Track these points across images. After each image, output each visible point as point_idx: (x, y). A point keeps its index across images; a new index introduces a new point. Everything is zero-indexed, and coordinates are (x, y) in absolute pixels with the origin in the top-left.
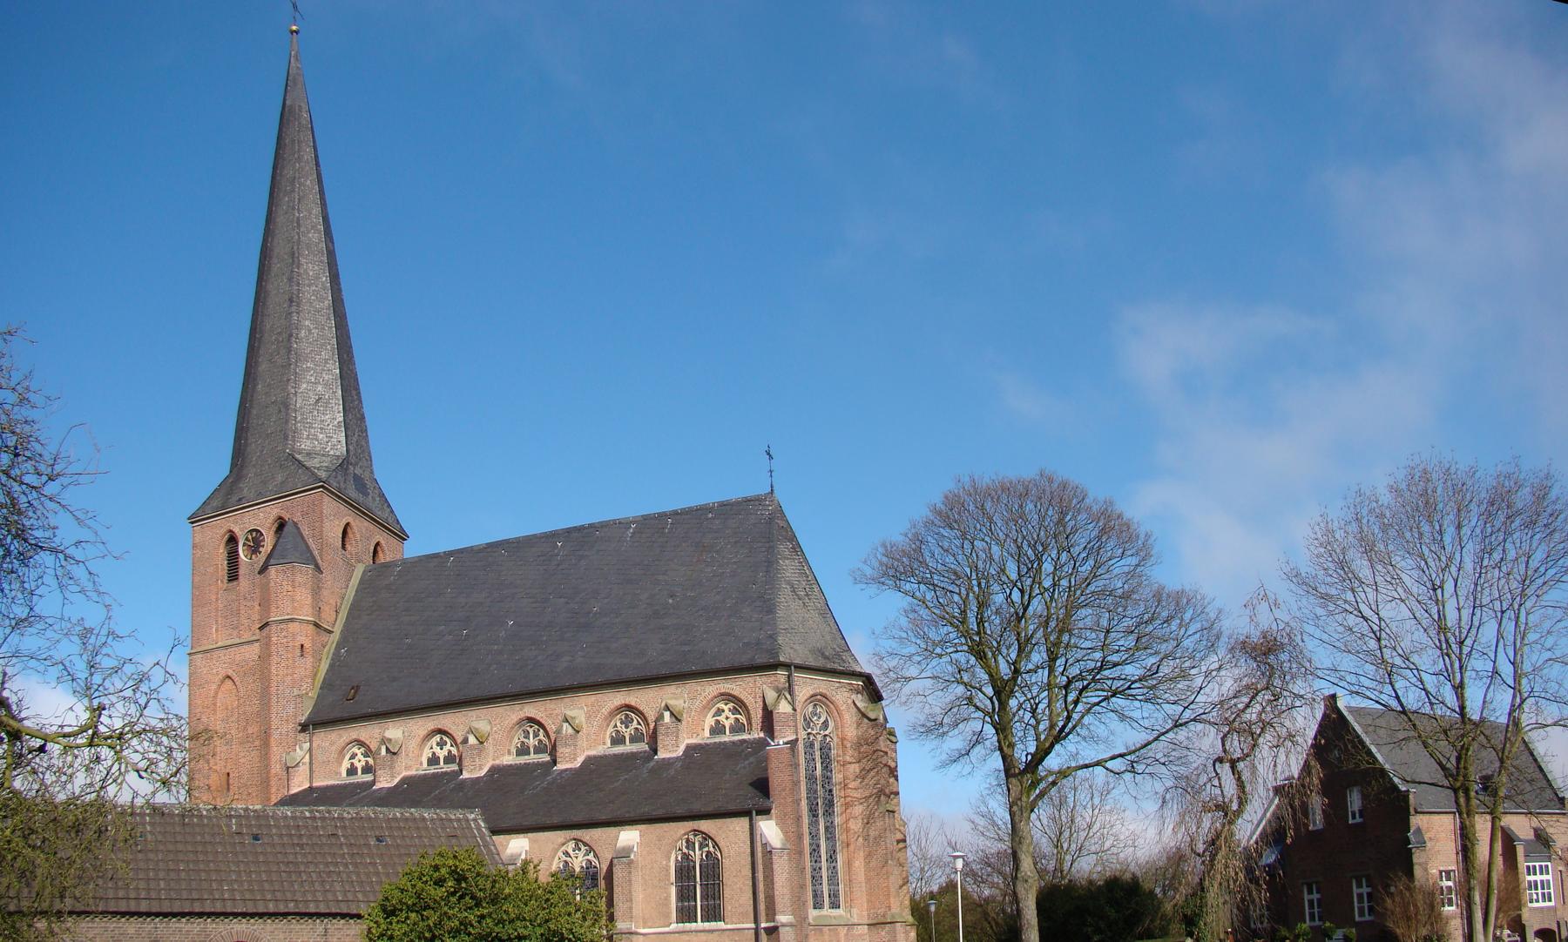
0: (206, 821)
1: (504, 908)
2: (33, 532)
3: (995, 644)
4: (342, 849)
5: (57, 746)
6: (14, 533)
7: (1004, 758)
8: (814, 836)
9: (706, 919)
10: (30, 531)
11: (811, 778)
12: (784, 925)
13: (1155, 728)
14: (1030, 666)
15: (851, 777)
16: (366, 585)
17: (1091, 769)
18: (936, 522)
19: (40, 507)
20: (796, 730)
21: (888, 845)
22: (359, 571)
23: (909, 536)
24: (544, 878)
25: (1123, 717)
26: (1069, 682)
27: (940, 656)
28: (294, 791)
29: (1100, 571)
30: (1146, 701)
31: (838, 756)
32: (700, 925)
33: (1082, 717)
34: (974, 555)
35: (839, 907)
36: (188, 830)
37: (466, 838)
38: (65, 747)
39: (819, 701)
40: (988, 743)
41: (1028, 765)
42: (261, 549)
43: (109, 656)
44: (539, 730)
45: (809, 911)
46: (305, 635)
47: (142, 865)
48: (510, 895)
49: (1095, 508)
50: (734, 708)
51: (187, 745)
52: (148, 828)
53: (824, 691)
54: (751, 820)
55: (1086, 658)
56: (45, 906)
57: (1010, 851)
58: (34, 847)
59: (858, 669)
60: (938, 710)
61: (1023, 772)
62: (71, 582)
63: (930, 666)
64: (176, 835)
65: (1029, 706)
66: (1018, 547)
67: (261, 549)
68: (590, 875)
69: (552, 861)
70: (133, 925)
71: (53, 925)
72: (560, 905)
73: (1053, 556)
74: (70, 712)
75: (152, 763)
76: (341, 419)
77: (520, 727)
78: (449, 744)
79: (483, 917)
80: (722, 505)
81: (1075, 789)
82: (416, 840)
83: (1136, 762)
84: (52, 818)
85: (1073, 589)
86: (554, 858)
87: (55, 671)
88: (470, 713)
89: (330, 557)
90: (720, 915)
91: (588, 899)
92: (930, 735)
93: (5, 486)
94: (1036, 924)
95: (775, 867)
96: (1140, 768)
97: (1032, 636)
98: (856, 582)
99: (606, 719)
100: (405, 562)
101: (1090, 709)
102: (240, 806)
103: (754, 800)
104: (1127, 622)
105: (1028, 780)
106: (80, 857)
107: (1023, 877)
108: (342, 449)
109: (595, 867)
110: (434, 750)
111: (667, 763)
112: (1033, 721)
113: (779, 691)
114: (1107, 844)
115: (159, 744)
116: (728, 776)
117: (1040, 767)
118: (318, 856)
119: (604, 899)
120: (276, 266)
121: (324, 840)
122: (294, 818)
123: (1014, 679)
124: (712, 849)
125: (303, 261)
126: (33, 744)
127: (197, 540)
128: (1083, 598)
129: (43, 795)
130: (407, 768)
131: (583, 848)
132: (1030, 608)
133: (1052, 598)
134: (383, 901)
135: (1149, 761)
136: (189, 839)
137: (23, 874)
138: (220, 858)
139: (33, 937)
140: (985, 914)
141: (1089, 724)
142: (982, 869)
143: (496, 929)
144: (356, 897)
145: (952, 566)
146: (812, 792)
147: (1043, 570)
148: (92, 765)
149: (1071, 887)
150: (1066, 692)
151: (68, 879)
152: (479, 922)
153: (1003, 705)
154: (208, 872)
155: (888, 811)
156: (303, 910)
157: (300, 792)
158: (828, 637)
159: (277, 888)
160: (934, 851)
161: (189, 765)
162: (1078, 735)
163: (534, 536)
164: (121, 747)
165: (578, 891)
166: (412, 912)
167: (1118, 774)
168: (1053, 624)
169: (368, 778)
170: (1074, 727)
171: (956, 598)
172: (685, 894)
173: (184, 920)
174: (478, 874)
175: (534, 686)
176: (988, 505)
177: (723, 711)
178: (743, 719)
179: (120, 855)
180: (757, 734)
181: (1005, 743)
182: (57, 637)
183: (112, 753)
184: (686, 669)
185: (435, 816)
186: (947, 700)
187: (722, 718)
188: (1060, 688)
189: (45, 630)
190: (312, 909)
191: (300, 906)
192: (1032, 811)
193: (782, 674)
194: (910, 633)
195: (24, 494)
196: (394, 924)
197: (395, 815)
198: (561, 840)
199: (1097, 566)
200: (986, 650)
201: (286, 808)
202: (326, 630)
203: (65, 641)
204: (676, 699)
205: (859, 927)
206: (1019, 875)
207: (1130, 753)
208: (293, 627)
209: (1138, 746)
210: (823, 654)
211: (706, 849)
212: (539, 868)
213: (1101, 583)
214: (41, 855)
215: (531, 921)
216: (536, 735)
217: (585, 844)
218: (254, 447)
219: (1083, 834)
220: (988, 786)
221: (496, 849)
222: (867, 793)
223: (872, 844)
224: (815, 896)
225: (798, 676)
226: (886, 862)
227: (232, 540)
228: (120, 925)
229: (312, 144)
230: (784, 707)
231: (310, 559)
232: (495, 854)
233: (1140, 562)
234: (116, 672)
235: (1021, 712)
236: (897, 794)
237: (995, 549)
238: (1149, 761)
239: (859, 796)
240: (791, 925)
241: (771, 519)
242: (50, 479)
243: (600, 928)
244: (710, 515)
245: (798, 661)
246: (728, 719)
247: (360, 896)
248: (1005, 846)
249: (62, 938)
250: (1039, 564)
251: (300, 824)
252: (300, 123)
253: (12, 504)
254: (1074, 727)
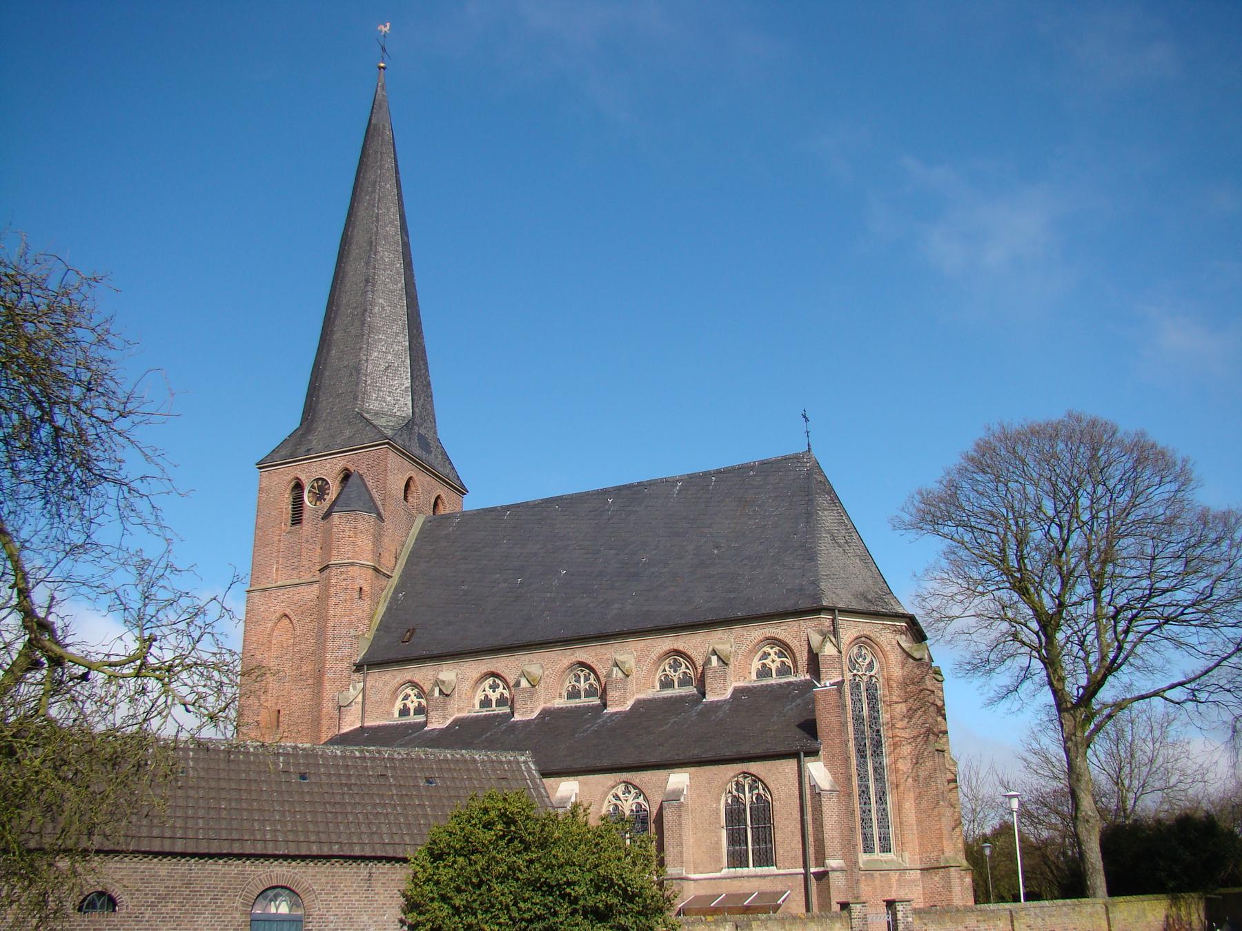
0: (252, 758)
1: (553, 852)
2: (99, 463)
3: (1037, 579)
4: (391, 790)
5: (101, 675)
6: (78, 462)
7: (1055, 692)
8: (863, 777)
9: (759, 862)
10: (95, 462)
11: (858, 719)
12: (834, 870)
13: (1215, 653)
14: (1074, 599)
15: (899, 717)
16: (426, 535)
17: (1148, 700)
18: (970, 468)
19: (108, 440)
20: (842, 671)
21: (939, 786)
22: (419, 521)
23: (945, 483)
24: (594, 822)
25: (1179, 644)
26: (1117, 612)
27: (983, 594)
28: (345, 730)
29: (1139, 500)
30: (1202, 625)
31: (884, 696)
32: (751, 870)
33: (1135, 646)
34: (1009, 496)
35: (890, 851)
36: (233, 767)
37: (517, 780)
38: (110, 676)
39: (864, 642)
40: (1036, 678)
41: (1080, 699)
42: (326, 497)
43: (165, 588)
44: (590, 674)
45: (859, 855)
46: (364, 579)
47: (181, 802)
48: (559, 839)
49: (1127, 441)
50: (780, 651)
51: (238, 681)
52: (191, 764)
53: (868, 633)
54: (799, 762)
55: (1133, 586)
56: (70, 843)
57: (1066, 790)
58: (64, 780)
59: (901, 611)
60: (983, 647)
61: (1075, 706)
62: (133, 514)
63: (972, 605)
64: (220, 771)
65: (1076, 638)
66: (1053, 485)
67: (326, 497)
68: (640, 819)
69: (603, 804)
70: (166, 866)
71: (77, 865)
72: (610, 849)
73: (1088, 490)
74: (119, 641)
75: (201, 696)
76: (409, 385)
78: (501, 687)
79: (531, 861)
80: (762, 463)
81: (1132, 722)
82: (467, 782)
83: (1197, 690)
84: (88, 749)
85: (1112, 520)
86: (603, 801)
87: (107, 600)
88: (523, 657)
89: (393, 507)
90: (772, 859)
91: (639, 843)
92: (976, 672)
93: (74, 417)
94: (1101, 868)
95: (824, 809)
96: (1202, 696)
97: (1074, 570)
98: (895, 528)
99: (655, 663)
100: (463, 514)
101: (1142, 637)
102: (288, 744)
103: (804, 741)
104: (1173, 548)
105: (1081, 714)
106: (115, 792)
107: (1084, 817)
108: (408, 411)
109: (645, 810)
110: (487, 693)
111: (716, 706)
112: (1081, 654)
113: (824, 635)
114: (1173, 780)
115: (210, 678)
116: (775, 718)
117: (1093, 700)
118: (366, 797)
119: (654, 843)
120: (355, 251)
121: (373, 781)
122: (344, 757)
123: (1060, 612)
124: (762, 792)
125: (380, 249)
126: (76, 671)
127: (264, 484)
128: (1123, 528)
129: (81, 725)
130: (459, 710)
131: (633, 791)
132: (1070, 541)
133: (1091, 530)
134: (431, 844)
135: (1212, 689)
136: (233, 776)
137: (49, 808)
138: (265, 797)
139: (52, 877)
140: (1045, 858)
141: (1143, 653)
142: (1038, 809)
143: (545, 875)
144: (403, 840)
145: (989, 508)
146: (859, 733)
147: (1080, 504)
148: (136, 696)
149: (1137, 826)
150: (1115, 623)
151: (99, 815)
152: (528, 867)
153: (1050, 639)
154: (250, 811)
155: (937, 750)
156: (348, 853)
157: (351, 731)
158: (870, 582)
159: (321, 829)
160: (986, 791)
161: (239, 701)
162: (1131, 665)
163: (587, 493)
164: (170, 679)
165: (628, 835)
166: (459, 856)
167: (1178, 703)
168: (1095, 556)
169: (421, 719)
170: (1126, 658)
171: (994, 538)
172: (736, 838)
173: (221, 862)
174: (528, 817)
175: (585, 632)
176: (1019, 449)
177: (769, 654)
178: (788, 662)
179: (158, 791)
180: (804, 676)
181: (1054, 677)
182: (113, 566)
183: (160, 685)
184: (731, 615)
185: (486, 758)
186: (992, 637)
187: (768, 661)
188: (1108, 619)
189: (101, 558)
190: (357, 851)
191: (345, 848)
192: (1088, 746)
193: (826, 619)
194: (951, 574)
195: (94, 426)
196: (441, 869)
197: (445, 756)
198: (611, 783)
199: (1136, 495)
200: (1029, 586)
201: (336, 747)
202: (385, 575)
203: (121, 571)
204: (722, 643)
205: (912, 872)
206: (1079, 815)
207: (1189, 682)
208: (353, 571)
209: (1198, 673)
210: (866, 598)
211: (756, 791)
212: (588, 811)
213: (1141, 512)
214: (72, 789)
215: (580, 866)
216: (587, 679)
217: (635, 787)
218: (325, 404)
219: (1145, 769)
220: (1039, 722)
221: (546, 792)
222: (915, 733)
223: (923, 784)
224: (865, 839)
225: (843, 620)
226: (938, 803)
227: (298, 486)
228: (152, 866)
229: (393, 156)
230: (829, 650)
231: (373, 508)
232: (545, 797)
233: (1179, 487)
234: (171, 604)
235: (1069, 645)
236: (946, 732)
237: (1030, 489)
238: (1212, 689)
239: (907, 736)
240: (842, 870)
241: (809, 474)
242: (121, 415)
243: (650, 873)
244: (752, 473)
245: (841, 605)
246: (774, 662)
247: (407, 839)
248: (1061, 784)
249: (85, 880)
250: (1075, 499)
251: (350, 763)
252: (383, 139)
253: (79, 434)
254: (1126, 658)
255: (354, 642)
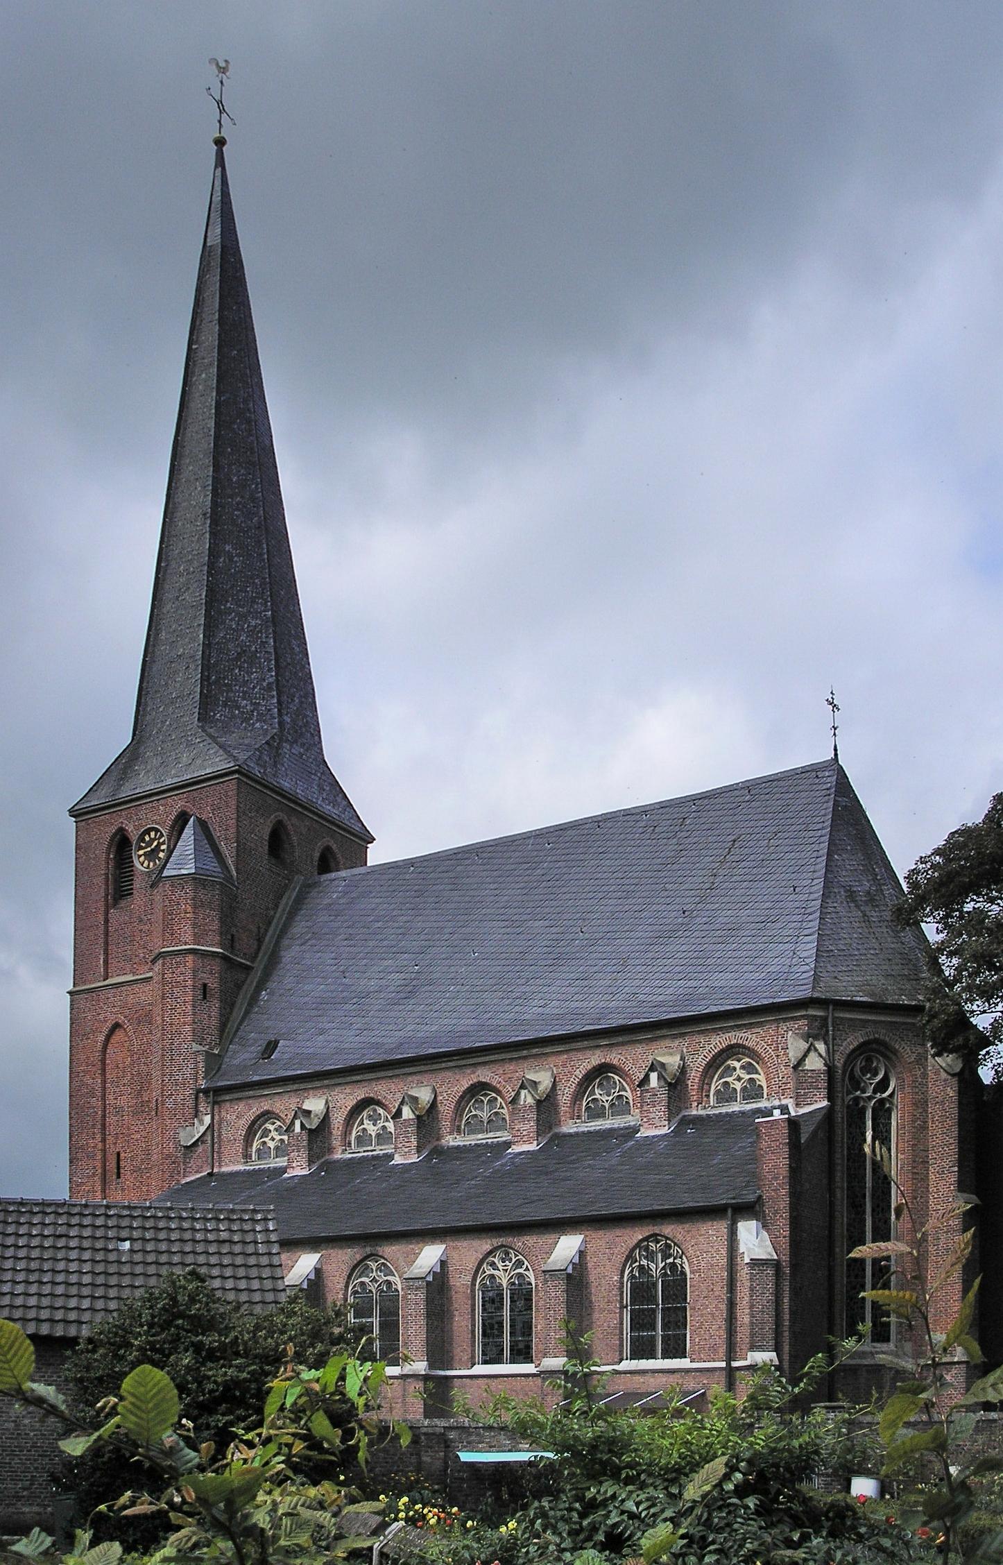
169: (281, 1162)
172: (641, 1321)
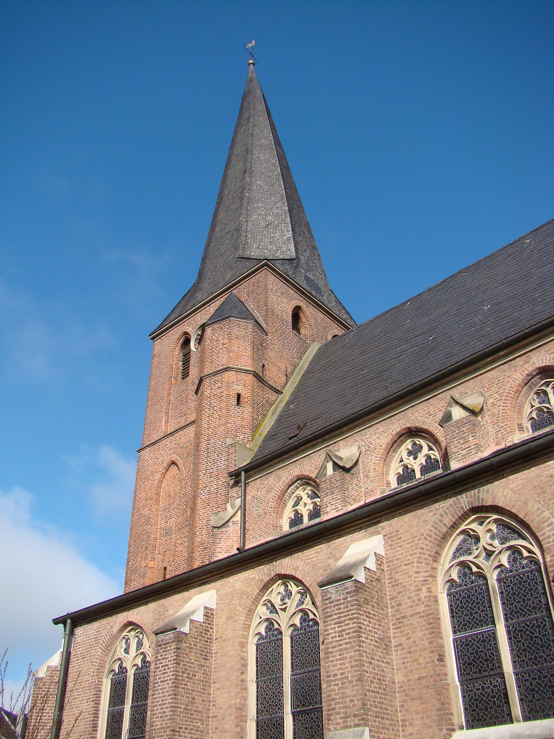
77: (531, 388)
110: (405, 461)
208: (229, 376)
255: (231, 452)
